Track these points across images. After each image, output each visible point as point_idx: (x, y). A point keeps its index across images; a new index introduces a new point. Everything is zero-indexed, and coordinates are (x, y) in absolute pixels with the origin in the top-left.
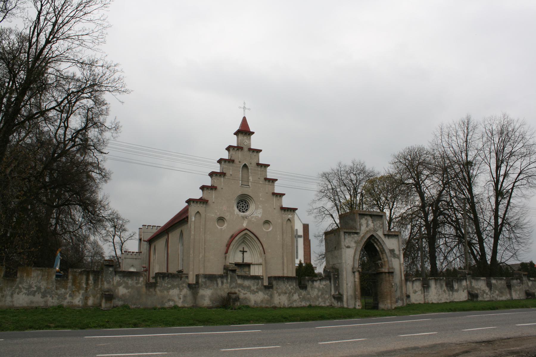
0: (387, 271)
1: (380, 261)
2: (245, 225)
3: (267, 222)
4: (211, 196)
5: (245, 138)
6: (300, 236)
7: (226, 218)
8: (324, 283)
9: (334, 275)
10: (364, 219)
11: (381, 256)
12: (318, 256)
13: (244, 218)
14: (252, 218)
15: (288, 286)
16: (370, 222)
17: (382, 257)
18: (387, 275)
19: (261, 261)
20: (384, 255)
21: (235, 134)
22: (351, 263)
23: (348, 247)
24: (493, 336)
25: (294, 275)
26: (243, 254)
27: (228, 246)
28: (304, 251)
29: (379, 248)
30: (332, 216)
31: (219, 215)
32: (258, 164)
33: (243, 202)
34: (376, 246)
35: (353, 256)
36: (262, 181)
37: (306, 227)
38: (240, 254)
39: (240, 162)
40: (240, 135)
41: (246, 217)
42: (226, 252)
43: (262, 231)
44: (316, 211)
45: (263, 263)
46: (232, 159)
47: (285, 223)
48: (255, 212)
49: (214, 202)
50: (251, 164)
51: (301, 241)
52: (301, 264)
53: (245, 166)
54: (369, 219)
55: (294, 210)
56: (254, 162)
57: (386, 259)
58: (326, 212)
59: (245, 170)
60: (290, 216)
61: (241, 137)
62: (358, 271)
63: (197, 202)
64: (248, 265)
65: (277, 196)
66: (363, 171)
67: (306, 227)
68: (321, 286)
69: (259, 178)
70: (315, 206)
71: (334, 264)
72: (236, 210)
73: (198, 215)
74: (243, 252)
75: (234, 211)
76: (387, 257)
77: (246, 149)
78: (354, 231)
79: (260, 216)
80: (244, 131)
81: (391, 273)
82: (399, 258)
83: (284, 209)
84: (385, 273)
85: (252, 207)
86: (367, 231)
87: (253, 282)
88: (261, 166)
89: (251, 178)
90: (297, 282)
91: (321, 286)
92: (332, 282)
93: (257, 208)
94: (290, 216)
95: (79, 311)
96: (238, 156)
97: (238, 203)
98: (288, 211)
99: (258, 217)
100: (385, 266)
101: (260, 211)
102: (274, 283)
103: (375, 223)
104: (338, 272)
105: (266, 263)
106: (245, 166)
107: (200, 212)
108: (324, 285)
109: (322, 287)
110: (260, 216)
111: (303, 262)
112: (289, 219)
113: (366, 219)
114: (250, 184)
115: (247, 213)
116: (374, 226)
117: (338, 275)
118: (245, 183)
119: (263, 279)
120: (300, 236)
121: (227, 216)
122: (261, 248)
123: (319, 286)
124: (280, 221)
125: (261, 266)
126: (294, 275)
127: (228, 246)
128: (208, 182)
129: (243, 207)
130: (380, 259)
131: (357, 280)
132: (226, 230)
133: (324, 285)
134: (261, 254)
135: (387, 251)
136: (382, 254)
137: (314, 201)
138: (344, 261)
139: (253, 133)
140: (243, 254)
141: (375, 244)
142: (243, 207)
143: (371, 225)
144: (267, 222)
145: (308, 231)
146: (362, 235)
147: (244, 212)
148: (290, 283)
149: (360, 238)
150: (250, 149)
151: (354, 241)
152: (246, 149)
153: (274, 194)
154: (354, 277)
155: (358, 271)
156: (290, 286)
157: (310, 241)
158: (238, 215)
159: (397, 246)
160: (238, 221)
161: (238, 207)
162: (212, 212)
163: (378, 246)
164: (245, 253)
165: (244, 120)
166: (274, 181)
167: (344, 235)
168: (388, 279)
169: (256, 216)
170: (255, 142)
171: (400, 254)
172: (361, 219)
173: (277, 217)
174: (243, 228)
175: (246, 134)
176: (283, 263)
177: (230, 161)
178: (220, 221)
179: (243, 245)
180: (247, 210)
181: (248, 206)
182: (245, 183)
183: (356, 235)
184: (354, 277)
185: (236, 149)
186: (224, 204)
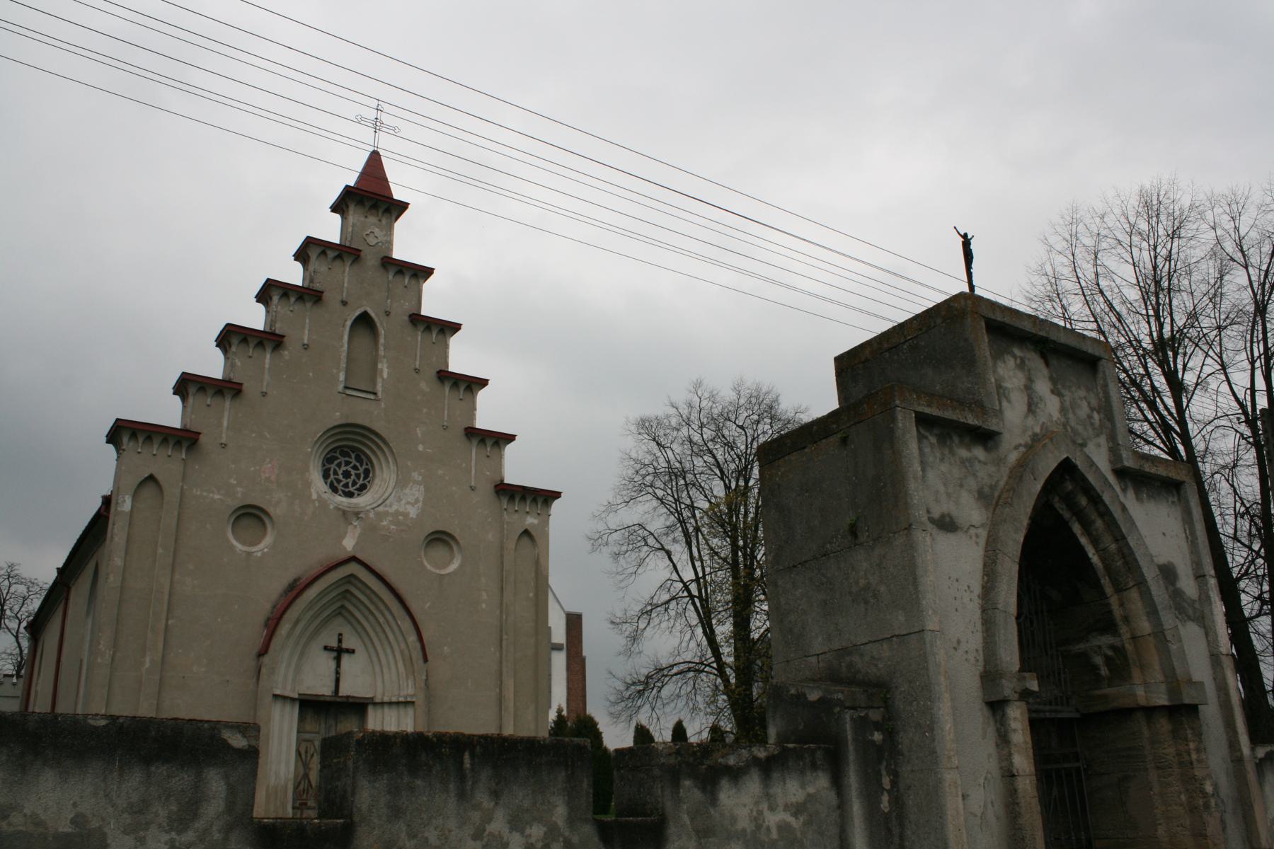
0: (1162, 700)
1: (1106, 640)
2: (349, 544)
3: (440, 538)
4: (220, 420)
5: (372, 219)
6: (558, 648)
7: (271, 510)
8: (792, 789)
9: (863, 725)
10: (1011, 362)
11: (1114, 601)
12: (621, 687)
13: (347, 516)
14: (381, 516)
15: (498, 825)
16: (1043, 387)
17: (1117, 612)
18: (1164, 725)
19: (411, 691)
20: (1134, 594)
21: (336, 208)
22: (974, 641)
23: (947, 524)
26: (338, 660)
28: (569, 689)
29: (1103, 559)
30: (669, 554)
31: (241, 496)
32: (418, 320)
33: (350, 455)
34: (1083, 540)
35: (977, 589)
36: (426, 385)
37: (574, 623)
38: (325, 663)
39: (344, 303)
40: (352, 208)
41: (357, 514)
42: (263, 652)
43: (424, 575)
44: (616, 536)
45: (420, 700)
46: (317, 286)
47: (511, 545)
48: (395, 497)
49: (224, 446)
50: (388, 314)
51: (559, 661)
52: (560, 720)
53: (365, 321)
54: (1035, 361)
56: (402, 309)
57: (1145, 626)
58: (651, 541)
59: (363, 339)
60: (531, 521)
61: (355, 215)
62: (1025, 695)
63: (149, 439)
64: (359, 707)
66: (770, 412)
67: (574, 623)
68: (772, 819)
69: (417, 371)
70: (614, 521)
71: (844, 652)
72: (318, 485)
73: (148, 492)
74: (339, 652)
75: (308, 484)
76: (1153, 612)
77: (371, 260)
78: (971, 420)
79: (413, 512)
80: (370, 198)
81: (1182, 713)
82: (1203, 620)
84: (1150, 711)
85: (384, 478)
86: (1035, 438)
87: (132, 784)
89: (384, 369)
90: (586, 784)
91: (772, 819)
92: (853, 779)
93: (402, 483)
94: (531, 521)
95: (694, 753)
96: (341, 279)
97: (329, 460)
98: (523, 499)
99: (406, 515)
100: (1143, 667)
101: (415, 493)
102: (368, 795)
103: (1068, 396)
104: (887, 704)
106: (365, 321)
107: (159, 477)
108: (797, 810)
109: (783, 828)
110: (413, 512)
111: (565, 713)
112: (526, 533)
113: (1021, 365)
114: (379, 388)
115: (362, 501)
116: (1063, 410)
117: (890, 727)
118: (360, 384)
119: (251, 755)
120: (558, 648)
121: (278, 504)
122: (412, 638)
123: (757, 820)
125: (410, 711)
127: (273, 624)
128: (213, 365)
130: (1109, 626)
131: (1023, 762)
132: (270, 560)
133: (797, 810)
134: (409, 662)
135: (1150, 574)
136: (1119, 589)
137: (611, 508)
138: (931, 625)
139: (402, 207)
140: (338, 660)
141: (1077, 528)
142: (347, 475)
143: (1051, 406)
144: (440, 538)
145: (580, 642)
146: (1013, 457)
147: (350, 495)
148: (520, 796)
149: (1005, 472)
150: (389, 263)
151: (972, 483)
152: (371, 260)
154: (1003, 738)
155: (1025, 695)
156: (516, 823)
157: (583, 661)
158: (323, 503)
159: (1185, 546)
160: (318, 521)
161: (326, 475)
162: (215, 487)
163: (1095, 542)
164: (346, 659)
165: (375, 160)
166: (475, 384)
167: (921, 438)
168: (1169, 750)
169: (397, 513)
170: (407, 242)
171: (1205, 598)
172: (998, 355)
173: (480, 523)
174: (343, 556)
175: (375, 207)
176: (500, 700)
177: (307, 295)
178: (245, 522)
179: (339, 626)
180: (363, 488)
181: (367, 472)
182: (360, 384)
183: (979, 452)
184: (1003, 738)
185: (331, 254)
186: (273, 461)
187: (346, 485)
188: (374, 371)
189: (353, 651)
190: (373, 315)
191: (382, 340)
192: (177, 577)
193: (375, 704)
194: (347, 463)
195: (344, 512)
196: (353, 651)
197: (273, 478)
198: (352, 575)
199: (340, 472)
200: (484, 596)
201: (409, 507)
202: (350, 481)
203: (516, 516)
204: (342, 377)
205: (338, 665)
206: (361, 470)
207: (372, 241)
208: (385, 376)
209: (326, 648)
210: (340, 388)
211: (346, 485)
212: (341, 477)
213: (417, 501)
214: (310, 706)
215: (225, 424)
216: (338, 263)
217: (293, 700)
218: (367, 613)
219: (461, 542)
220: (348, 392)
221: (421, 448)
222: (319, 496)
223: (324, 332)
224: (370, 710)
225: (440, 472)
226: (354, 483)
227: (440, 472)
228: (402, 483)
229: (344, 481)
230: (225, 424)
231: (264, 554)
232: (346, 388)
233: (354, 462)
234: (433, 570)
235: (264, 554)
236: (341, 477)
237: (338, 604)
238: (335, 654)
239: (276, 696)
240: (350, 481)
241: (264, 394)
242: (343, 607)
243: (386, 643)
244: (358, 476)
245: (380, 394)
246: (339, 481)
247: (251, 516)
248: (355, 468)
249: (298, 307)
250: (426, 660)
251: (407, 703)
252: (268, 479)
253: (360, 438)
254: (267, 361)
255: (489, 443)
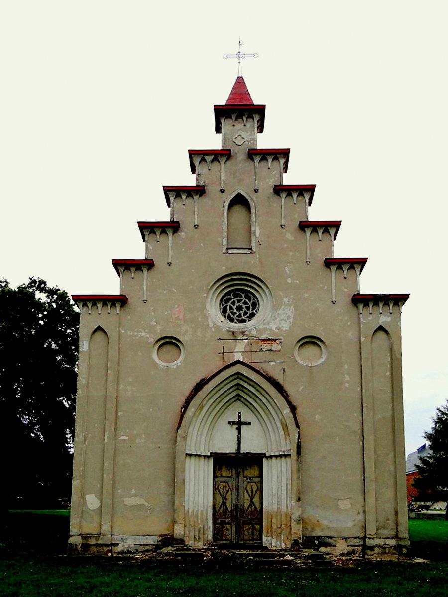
3: (310, 341)
5: (239, 126)
24: (358, 472)
25: (242, 452)
26: (239, 429)
27: (186, 406)
36: (290, 234)
43: (299, 370)
46: (202, 183)
48: (273, 318)
49: (145, 301)
55: (401, 299)
60: (384, 320)
65: (289, 194)
72: (214, 311)
74: (239, 424)
79: (286, 326)
83: (361, 300)
88: (289, 194)
93: (276, 308)
97: (224, 300)
98: (376, 304)
105: (299, 453)
112: (381, 329)
114: (254, 245)
124: (352, 335)
126: (242, 452)
127: (186, 406)
128: (137, 250)
129: (239, 309)
132: (183, 370)
140: (239, 429)
142: (239, 309)
144: (310, 341)
153: (330, 263)
164: (244, 428)
165: (240, 82)
166: (331, 227)
173: (340, 326)
178: (167, 348)
179: (238, 407)
180: (252, 316)
181: (254, 305)
185: (209, 158)
187: (240, 316)
188: (250, 233)
189: (250, 423)
190: (245, 194)
191: (253, 211)
192: (121, 386)
193: (268, 457)
194: (239, 301)
195: (233, 333)
196: (250, 423)
197: (181, 317)
198: (238, 373)
199: (235, 308)
200: (347, 378)
201: (282, 323)
202: (242, 312)
203: (371, 318)
204: (225, 242)
205: (239, 433)
206: (250, 304)
207: (239, 141)
208: (258, 235)
209: (230, 423)
210: (224, 249)
211: (240, 316)
212: (235, 311)
213: (289, 318)
214: (220, 461)
215: (145, 288)
216: (216, 164)
217: (208, 457)
218: (255, 397)
219: (185, 346)
220: (230, 251)
221: (289, 280)
222: (214, 324)
223: (211, 212)
224: (265, 460)
225: (306, 295)
226: (245, 314)
227: (306, 295)
228: (276, 308)
229: (238, 313)
230: (145, 288)
231: (178, 367)
232: (228, 249)
233: (244, 299)
234: (301, 362)
235: (178, 367)
236: (235, 311)
237: (235, 393)
238: (236, 426)
239: (186, 454)
240: (242, 312)
241: (169, 264)
242: (238, 395)
243: (270, 416)
244: (248, 308)
245: (254, 249)
246: (234, 314)
247: (169, 342)
248: (245, 303)
249: (189, 201)
250: (298, 426)
251: (286, 456)
252: (177, 318)
253: (252, 279)
254: (283, 202)
255: (346, 267)
